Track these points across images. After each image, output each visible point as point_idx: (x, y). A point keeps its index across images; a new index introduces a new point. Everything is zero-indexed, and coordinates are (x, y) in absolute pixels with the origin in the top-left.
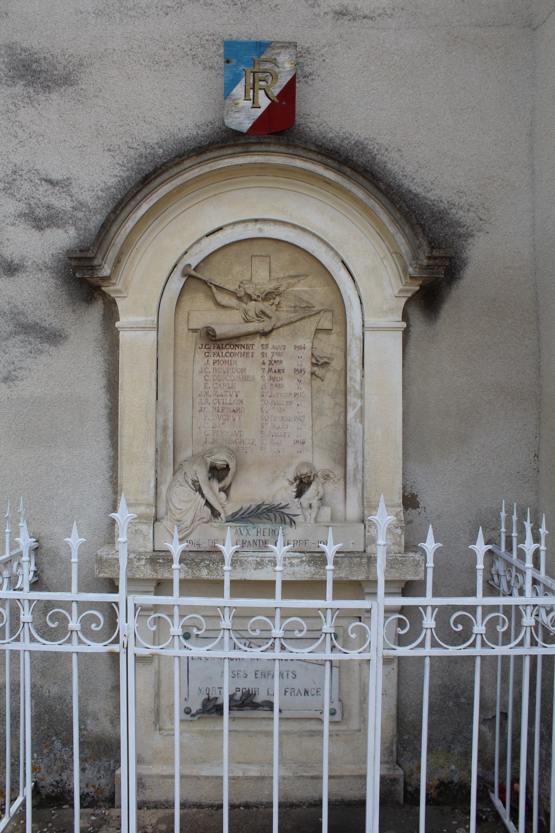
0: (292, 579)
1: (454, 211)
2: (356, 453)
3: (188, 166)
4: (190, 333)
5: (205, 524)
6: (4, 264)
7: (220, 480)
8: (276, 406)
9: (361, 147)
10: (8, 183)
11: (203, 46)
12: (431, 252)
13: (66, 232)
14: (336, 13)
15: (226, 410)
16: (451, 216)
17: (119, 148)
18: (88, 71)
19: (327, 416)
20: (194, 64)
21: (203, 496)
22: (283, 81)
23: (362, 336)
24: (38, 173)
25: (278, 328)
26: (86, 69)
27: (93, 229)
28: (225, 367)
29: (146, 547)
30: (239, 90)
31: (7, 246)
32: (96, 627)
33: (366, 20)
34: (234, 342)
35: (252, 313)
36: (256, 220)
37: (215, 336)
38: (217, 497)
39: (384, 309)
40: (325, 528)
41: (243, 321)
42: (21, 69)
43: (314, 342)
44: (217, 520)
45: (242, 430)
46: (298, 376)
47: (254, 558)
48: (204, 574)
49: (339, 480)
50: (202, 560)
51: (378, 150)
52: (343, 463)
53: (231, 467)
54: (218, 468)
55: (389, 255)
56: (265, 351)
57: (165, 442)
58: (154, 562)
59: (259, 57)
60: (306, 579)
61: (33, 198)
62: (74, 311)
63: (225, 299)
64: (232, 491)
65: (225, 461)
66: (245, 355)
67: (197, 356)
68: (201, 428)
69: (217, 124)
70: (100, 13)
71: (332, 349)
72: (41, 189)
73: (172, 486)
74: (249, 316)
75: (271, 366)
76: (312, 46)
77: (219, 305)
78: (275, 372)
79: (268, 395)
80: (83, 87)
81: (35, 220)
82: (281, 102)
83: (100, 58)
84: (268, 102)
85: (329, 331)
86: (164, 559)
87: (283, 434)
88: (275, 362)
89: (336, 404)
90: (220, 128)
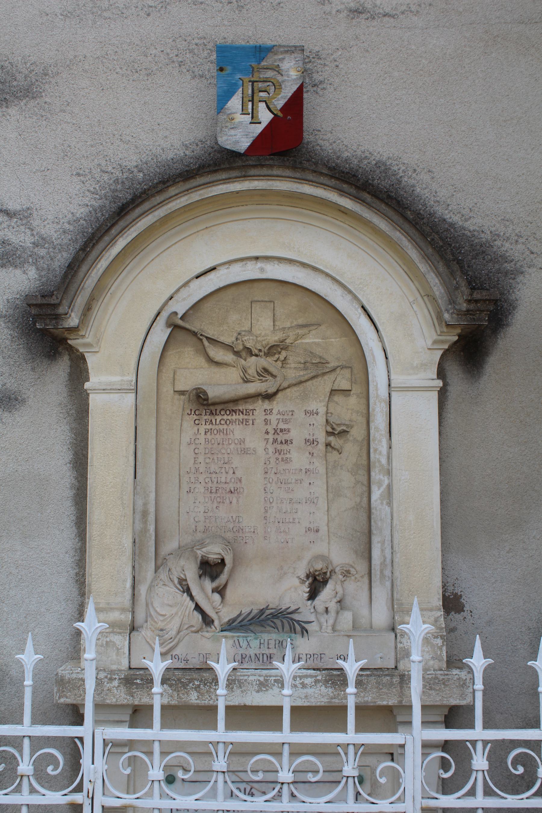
0: (305, 704)
1: (498, 243)
2: (383, 543)
3: (173, 194)
4: (177, 396)
5: (194, 634)
7: (213, 578)
8: (283, 486)
11: (191, 51)
12: (471, 295)
13: (24, 272)
15: (220, 490)
17: (90, 172)
18: (53, 81)
19: (346, 497)
21: (192, 598)
22: (288, 91)
23: (388, 398)
25: (285, 389)
26: (51, 79)
27: (57, 269)
28: (219, 437)
29: (120, 663)
33: (386, 19)
34: (231, 406)
35: (252, 371)
36: (257, 258)
37: (207, 399)
38: (209, 599)
39: (415, 365)
40: (346, 637)
41: (241, 381)
43: (329, 405)
44: (209, 629)
45: (241, 515)
46: (310, 448)
47: (255, 678)
48: (193, 698)
49: (362, 577)
50: (191, 680)
51: (404, 171)
52: (367, 555)
53: (227, 561)
54: (211, 563)
55: (420, 299)
57: (145, 530)
58: (129, 683)
60: (323, 704)
62: (33, 369)
64: (229, 592)
65: (220, 554)
66: (244, 423)
67: (185, 424)
68: (190, 513)
69: (208, 143)
70: (69, 15)
71: (352, 413)
73: (154, 586)
74: (249, 375)
75: (276, 436)
77: (211, 361)
78: (281, 443)
79: (273, 472)
80: (47, 100)
82: (285, 116)
83: (68, 66)
85: (348, 393)
86: (142, 680)
87: (291, 520)
88: (281, 430)
89: (358, 482)
90: (212, 148)
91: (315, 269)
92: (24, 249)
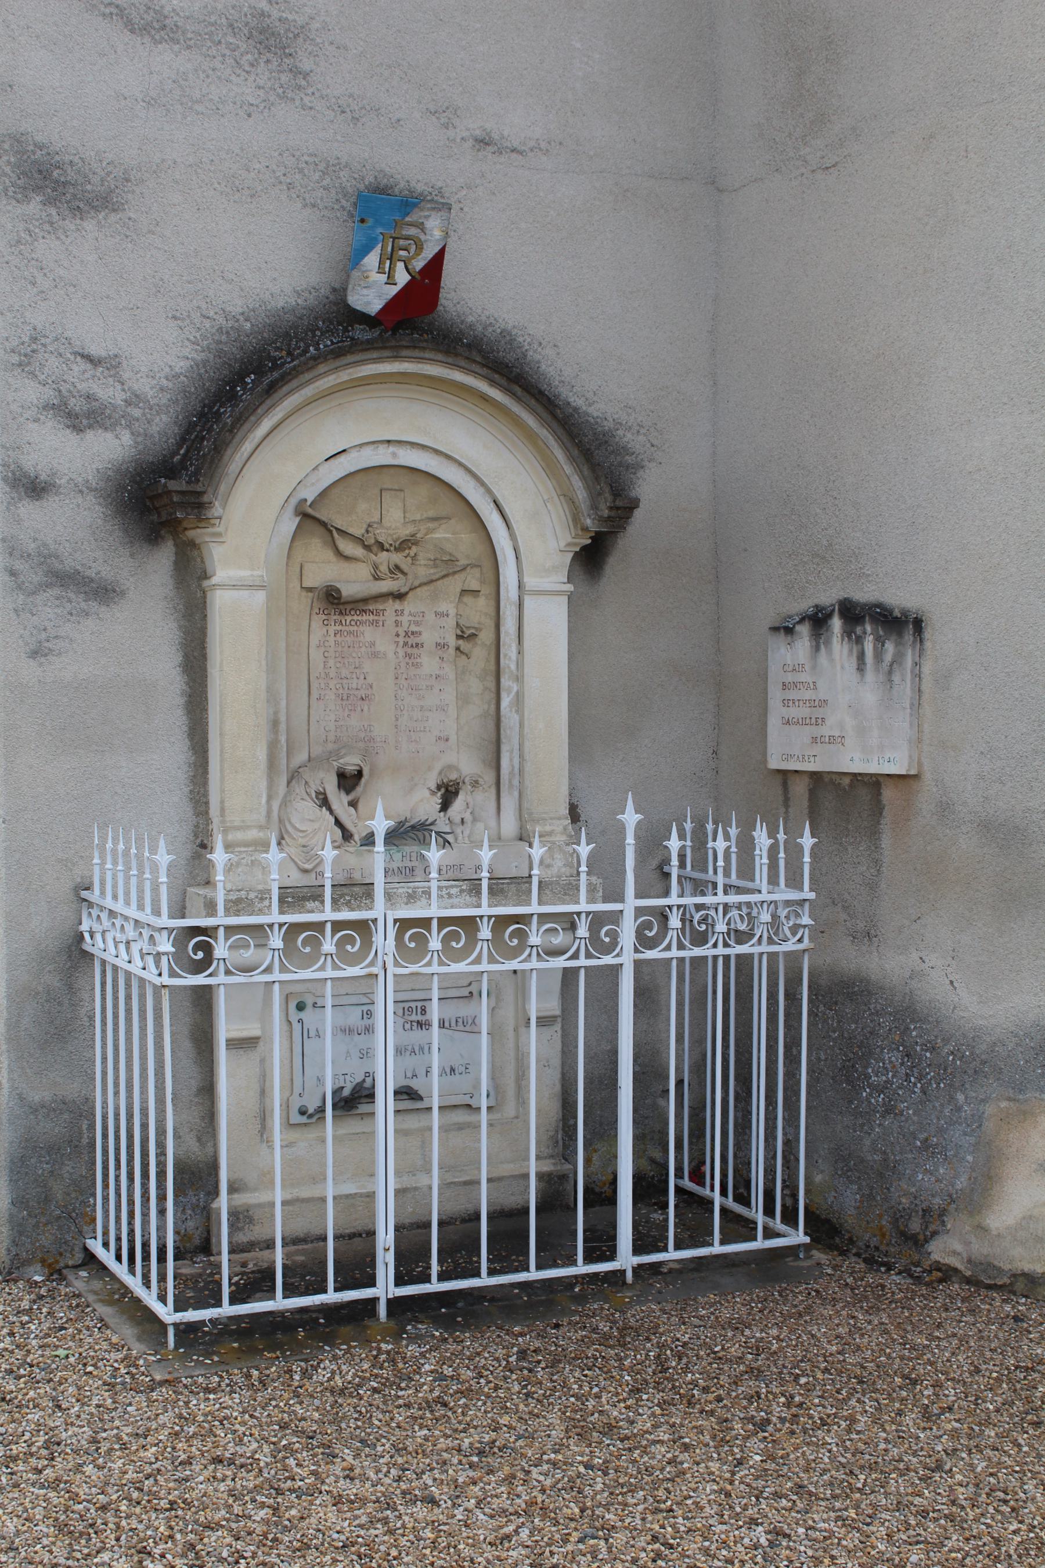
1: (620, 432)
2: (512, 752)
3: (322, 371)
4: (304, 593)
6: (25, 481)
9: (508, 338)
10: (26, 355)
11: (301, 171)
12: (614, 501)
13: (117, 437)
14: (476, 140)
16: (617, 440)
17: (189, 316)
18: (138, 191)
20: (290, 198)
22: (429, 252)
24: (70, 344)
25: (416, 588)
26: (135, 188)
27: (156, 435)
28: (349, 639)
30: (372, 260)
31: (28, 454)
32: (353, 946)
33: (514, 155)
34: (361, 606)
35: (384, 568)
36: (389, 442)
37: (339, 598)
41: (371, 578)
42: (36, 176)
46: (440, 652)
51: (529, 344)
55: (556, 498)
56: (399, 618)
59: (403, 219)
61: (65, 381)
62: (132, 555)
63: (347, 547)
64: (360, 806)
67: (314, 624)
69: (322, 291)
70: (152, 102)
72: (74, 367)
75: (407, 639)
76: (447, 186)
77: (339, 554)
80: (132, 215)
81: (70, 415)
82: (423, 279)
83: (155, 172)
84: (408, 278)
86: (293, 898)
88: (413, 633)
89: (486, 688)
90: (327, 298)
91: (448, 457)
92: (115, 407)
